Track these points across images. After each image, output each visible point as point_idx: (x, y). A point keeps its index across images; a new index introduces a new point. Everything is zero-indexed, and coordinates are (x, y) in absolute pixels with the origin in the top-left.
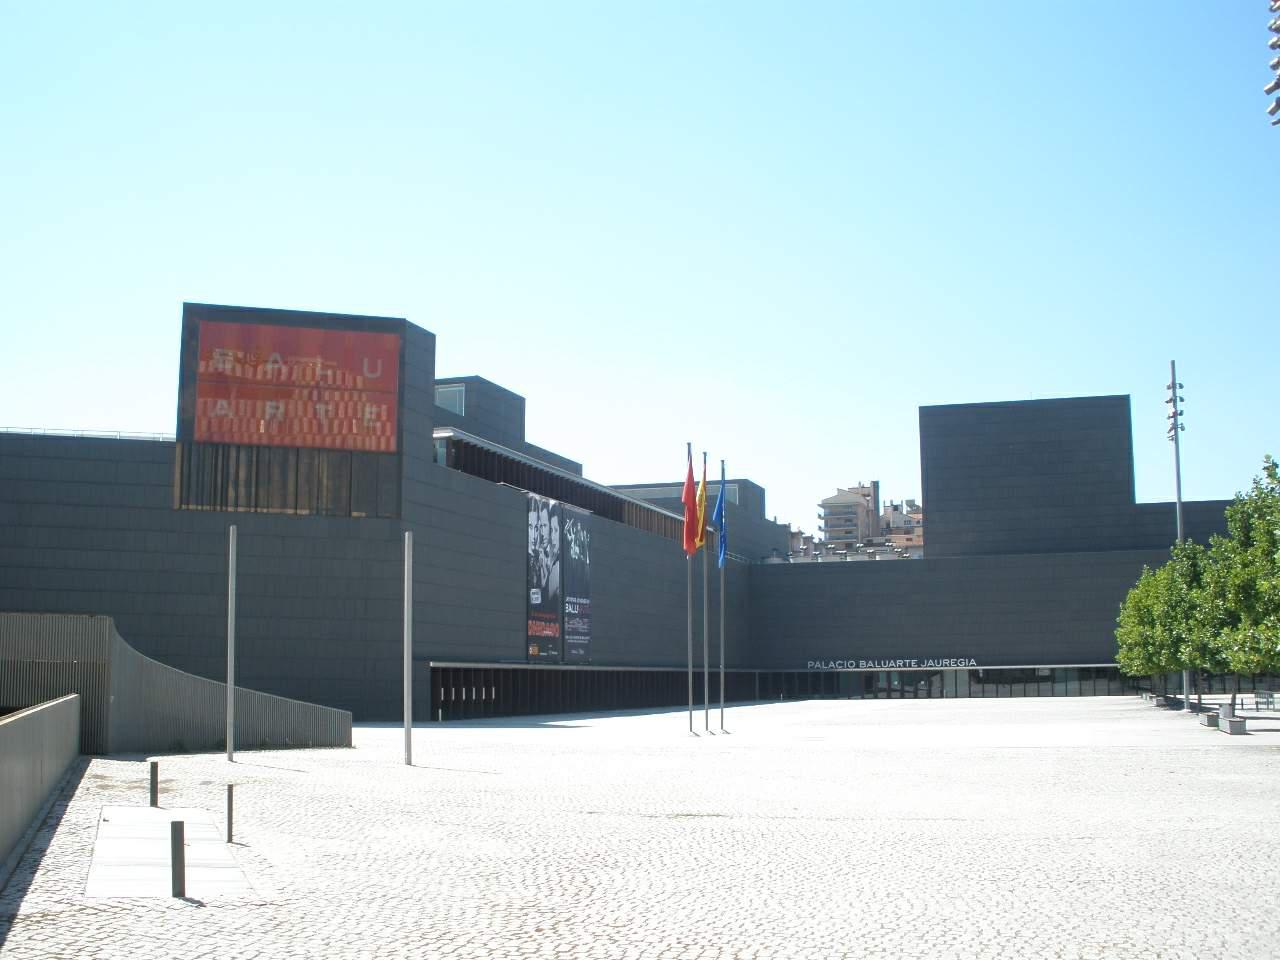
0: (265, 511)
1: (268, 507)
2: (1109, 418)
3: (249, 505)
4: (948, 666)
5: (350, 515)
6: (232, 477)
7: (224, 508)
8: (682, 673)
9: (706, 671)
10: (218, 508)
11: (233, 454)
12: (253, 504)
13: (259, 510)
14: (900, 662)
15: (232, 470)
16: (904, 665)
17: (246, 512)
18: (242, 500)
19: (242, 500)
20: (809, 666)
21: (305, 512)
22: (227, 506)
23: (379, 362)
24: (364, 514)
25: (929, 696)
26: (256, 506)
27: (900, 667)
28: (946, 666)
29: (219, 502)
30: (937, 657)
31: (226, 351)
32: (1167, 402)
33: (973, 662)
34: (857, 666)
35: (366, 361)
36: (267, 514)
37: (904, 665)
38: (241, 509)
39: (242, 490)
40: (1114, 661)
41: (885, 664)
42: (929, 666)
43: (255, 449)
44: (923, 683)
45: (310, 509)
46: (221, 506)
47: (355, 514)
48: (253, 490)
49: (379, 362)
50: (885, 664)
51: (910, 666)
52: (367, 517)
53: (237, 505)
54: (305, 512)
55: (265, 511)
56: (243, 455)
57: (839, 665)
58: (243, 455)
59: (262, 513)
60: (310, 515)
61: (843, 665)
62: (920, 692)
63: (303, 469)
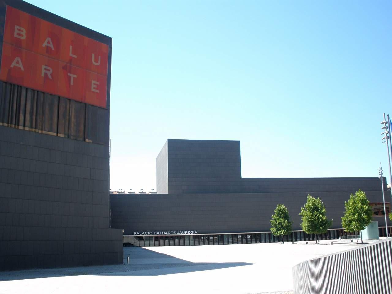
0: (40, 132)
1: (42, 130)
2: (230, 151)
3: (31, 127)
4: (186, 234)
5: (84, 140)
6: (22, 107)
7: (17, 126)
8: (389, 226)
9: (386, 227)
10: (13, 126)
11: (24, 93)
12: (34, 126)
13: (37, 130)
14: (169, 232)
15: (23, 103)
16: (171, 233)
17: (29, 131)
18: (28, 123)
19: (28, 123)
20: (134, 233)
21: (62, 136)
22: (18, 125)
23: (100, 57)
24: (91, 141)
25: (233, 243)
26: (35, 128)
27: (169, 234)
28: (186, 234)
29: (14, 122)
30: (183, 231)
31: (22, 29)
32: (382, 128)
33: (196, 232)
34: (153, 234)
35: (93, 55)
36: (42, 133)
37: (171, 233)
38: (27, 129)
39: (28, 116)
40: (302, 230)
41: (163, 233)
42: (180, 234)
43: (36, 92)
44: (167, 240)
45: (65, 134)
46: (15, 125)
47: (87, 140)
48: (34, 117)
49: (100, 57)
50: (163, 233)
51: (173, 234)
52: (92, 143)
53: (24, 126)
54: (62, 136)
55: (40, 132)
56: (29, 94)
57: (146, 233)
58: (29, 94)
59: (39, 133)
60: (65, 137)
61: (148, 233)
62: (210, 243)
63: (62, 109)
